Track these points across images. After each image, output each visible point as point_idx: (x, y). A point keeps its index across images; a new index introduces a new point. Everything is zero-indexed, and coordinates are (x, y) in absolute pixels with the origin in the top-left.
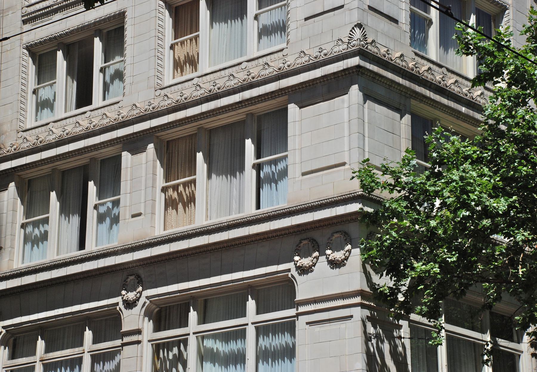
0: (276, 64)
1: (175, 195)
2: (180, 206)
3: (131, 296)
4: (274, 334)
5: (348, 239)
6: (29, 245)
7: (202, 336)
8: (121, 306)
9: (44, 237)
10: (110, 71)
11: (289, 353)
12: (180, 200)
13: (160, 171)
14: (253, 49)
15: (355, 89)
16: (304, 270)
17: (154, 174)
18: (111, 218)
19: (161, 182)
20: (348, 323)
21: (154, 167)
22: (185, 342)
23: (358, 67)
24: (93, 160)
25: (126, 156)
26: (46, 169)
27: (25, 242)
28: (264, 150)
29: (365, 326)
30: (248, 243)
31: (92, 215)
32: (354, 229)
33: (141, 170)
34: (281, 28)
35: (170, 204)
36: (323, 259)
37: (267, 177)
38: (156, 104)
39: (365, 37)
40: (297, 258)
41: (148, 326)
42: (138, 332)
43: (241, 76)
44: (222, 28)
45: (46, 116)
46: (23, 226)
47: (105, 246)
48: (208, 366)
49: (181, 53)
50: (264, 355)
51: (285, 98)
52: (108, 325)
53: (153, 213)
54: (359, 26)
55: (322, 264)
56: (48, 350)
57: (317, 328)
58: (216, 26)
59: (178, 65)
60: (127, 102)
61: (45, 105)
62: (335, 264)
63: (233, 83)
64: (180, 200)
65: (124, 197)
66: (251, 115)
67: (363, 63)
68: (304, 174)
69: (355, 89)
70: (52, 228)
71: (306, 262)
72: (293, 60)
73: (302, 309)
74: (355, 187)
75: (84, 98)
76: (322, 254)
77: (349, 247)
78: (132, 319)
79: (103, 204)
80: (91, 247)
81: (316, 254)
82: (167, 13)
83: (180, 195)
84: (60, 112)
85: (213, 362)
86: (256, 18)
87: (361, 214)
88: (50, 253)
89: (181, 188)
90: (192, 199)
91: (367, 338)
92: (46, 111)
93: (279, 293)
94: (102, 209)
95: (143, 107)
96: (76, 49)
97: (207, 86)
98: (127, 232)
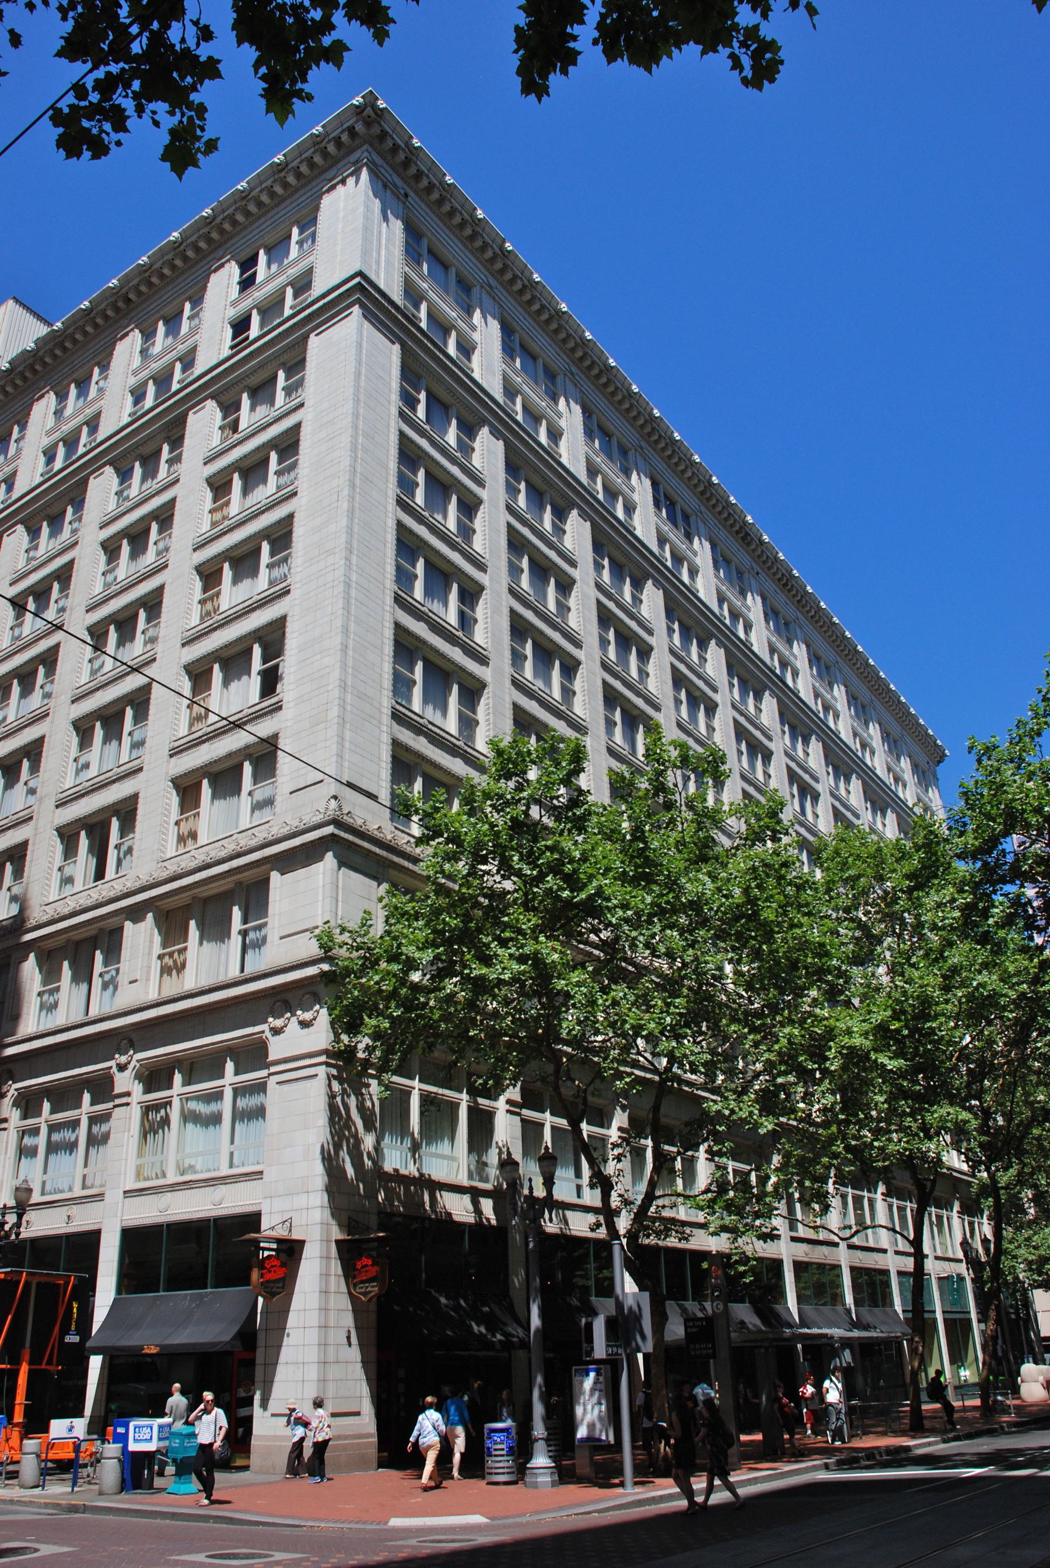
0: (262, 835)
1: (171, 963)
2: (174, 972)
3: (123, 1059)
4: (250, 1095)
5: (317, 999)
6: (44, 1012)
7: (186, 1098)
8: (115, 1069)
9: (55, 1005)
10: (124, 848)
11: (259, 1113)
12: (173, 968)
13: (157, 939)
14: (245, 822)
15: (329, 855)
16: (276, 1031)
17: (151, 942)
18: (111, 985)
19: (157, 949)
20: (314, 1081)
21: (152, 936)
22: (170, 1103)
23: (333, 835)
24: (101, 930)
25: (128, 925)
26: (61, 939)
27: (41, 1010)
28: (250, 917)
29: (330, 1086)
30: (228, 1006)
31: (97, 982)
32: (321, 989)
33: (141, 939)
34: (269, 802)
35: (166, 970)
36: (294, 1019)
37: (252, 941)
38: (155, 875)
39: (340, 808)
40: (270, 1019)
41: (137, 1089)
42: (128, 1094)
43: (230, 847)
44: (220, 804)
45: (68, 890)
46: (40, 994)
47: (107, 1010)
48: (190, 1126)
49: (185, 828)
50: (239, 1116)
51: (268, 866)
52: (102, 1088)
53: (148, 980)
54: (335, 797)
55: (293, 1024)
56: (53, 1111)
57: (286, 1087)
58: (216, 802)
59: (181, 839)
60: (132, 874)
61: (69, 880)
62: (305, 1024)
63: (223, 854)
64: (173, 968)
65: (125, 965)
66: (239, 883)
67: (337, 832)
68: (281, 938)
69: (329, 855)
70: (63, 996)
71: (278, 1023)
72: (277, 831)
73: (273, 1069)
74: (313, 949)
75: (100, 874)
76: (294, 1014)
77: (317, 1007)
78: (124, 1081)
79: (107, 972)
80: (94, 1012)
81: (288, 1015)
82: (174, 792)
83: (175, 962)
84: (78, 886)
85: (195, 1123)
86: (250, 794)
87: (323, 974)
88: (60, 1019)
89: (176, 955)
90: (184, 965)
91: (332, 1096)
92: (69, 886)
93: (253, 1055)
94: (107, 977)
95: (145, 879)
96: (96, 828)
97: (201, 857)
98: (127, 996)
